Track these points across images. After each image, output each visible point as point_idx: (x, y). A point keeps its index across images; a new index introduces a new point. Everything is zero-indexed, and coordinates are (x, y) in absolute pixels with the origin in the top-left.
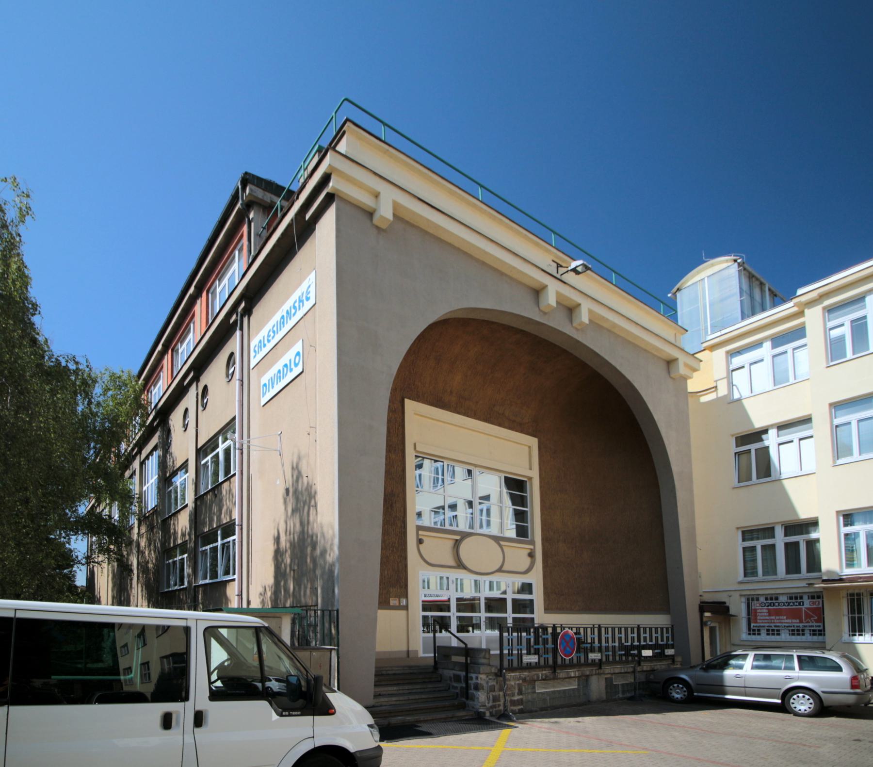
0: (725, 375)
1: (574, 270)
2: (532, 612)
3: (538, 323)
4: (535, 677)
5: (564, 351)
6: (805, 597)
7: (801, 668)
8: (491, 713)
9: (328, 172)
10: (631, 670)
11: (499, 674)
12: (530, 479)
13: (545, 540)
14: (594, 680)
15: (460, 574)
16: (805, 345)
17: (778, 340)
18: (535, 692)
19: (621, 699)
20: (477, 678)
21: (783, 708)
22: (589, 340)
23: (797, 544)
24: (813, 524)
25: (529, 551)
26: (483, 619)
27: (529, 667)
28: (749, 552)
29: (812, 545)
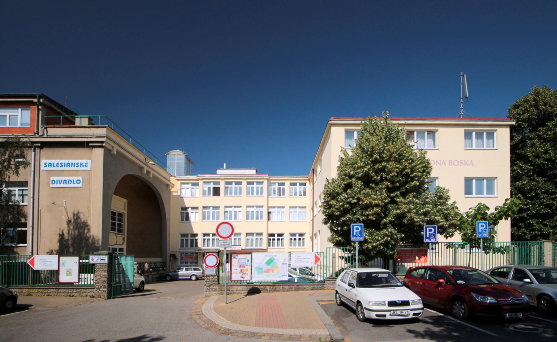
17: (193, 185)
21: (190, 279)
22: (152, 182)
24: (197, 235)
28: (182, 240)
29: (196, 240)
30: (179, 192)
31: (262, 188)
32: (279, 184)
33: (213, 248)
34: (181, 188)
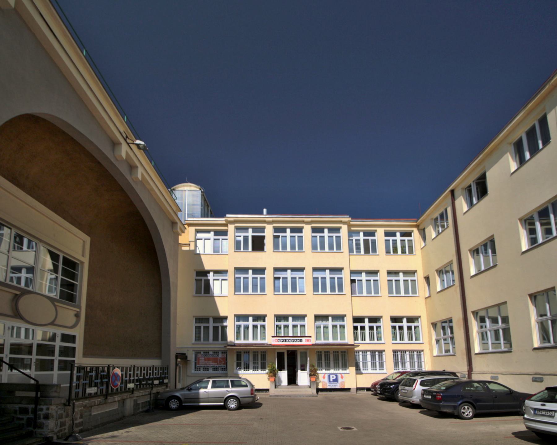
0: (194, 240)
1: (138, 145)
2: (74, 356)
3: (112, 163)
4: (93, 404)
6: (220, 352)
7: (232, 387)
8: (57, 436)
10: (147, 393)
11: (69, 402)
13: (88, 306)
15: (17, 323)
16: (227, 239)
17: (217, 233)
18: (90, 415)
19: (142, 412)
20: (48, 409)
23: (218, 327)
24: (226, 318)
25: (76, 313)
26: (34, 361)
27: (91, 396)
28: (198, 328)
30: (192, 245)
31: (338, 238)
32: (366, 234)
33: (255, 342)
34: (196, 239)
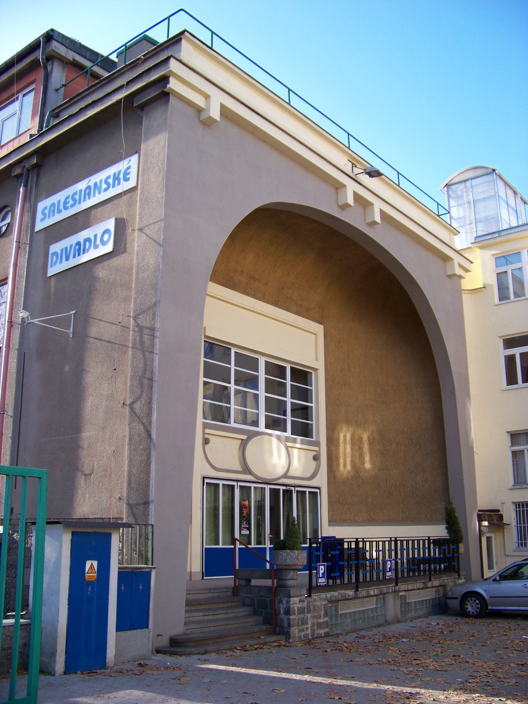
5: (356, 244)
9: (168, 75)
12: (316, 370)
14: (390, 598)
25: (314, 453)
